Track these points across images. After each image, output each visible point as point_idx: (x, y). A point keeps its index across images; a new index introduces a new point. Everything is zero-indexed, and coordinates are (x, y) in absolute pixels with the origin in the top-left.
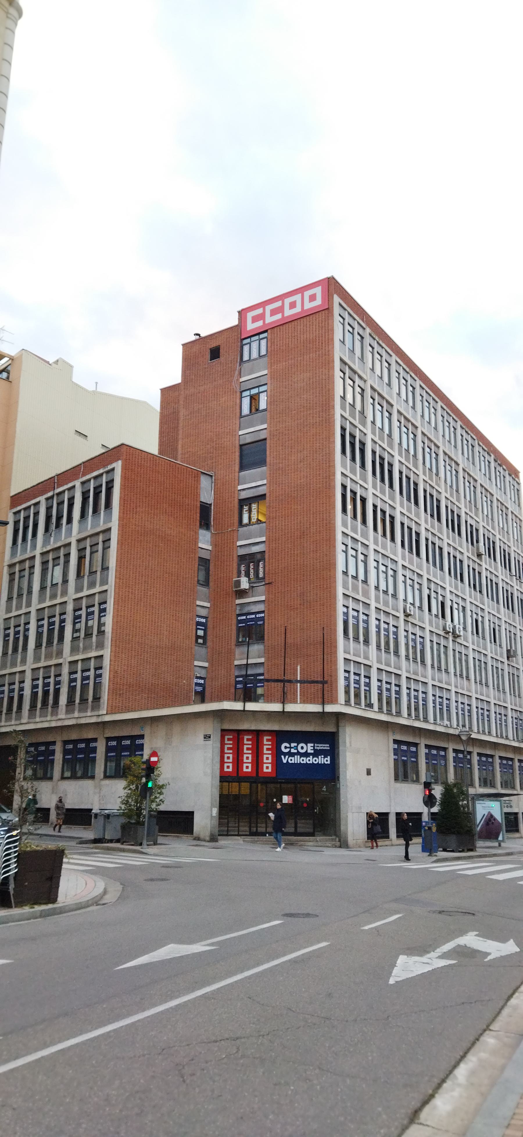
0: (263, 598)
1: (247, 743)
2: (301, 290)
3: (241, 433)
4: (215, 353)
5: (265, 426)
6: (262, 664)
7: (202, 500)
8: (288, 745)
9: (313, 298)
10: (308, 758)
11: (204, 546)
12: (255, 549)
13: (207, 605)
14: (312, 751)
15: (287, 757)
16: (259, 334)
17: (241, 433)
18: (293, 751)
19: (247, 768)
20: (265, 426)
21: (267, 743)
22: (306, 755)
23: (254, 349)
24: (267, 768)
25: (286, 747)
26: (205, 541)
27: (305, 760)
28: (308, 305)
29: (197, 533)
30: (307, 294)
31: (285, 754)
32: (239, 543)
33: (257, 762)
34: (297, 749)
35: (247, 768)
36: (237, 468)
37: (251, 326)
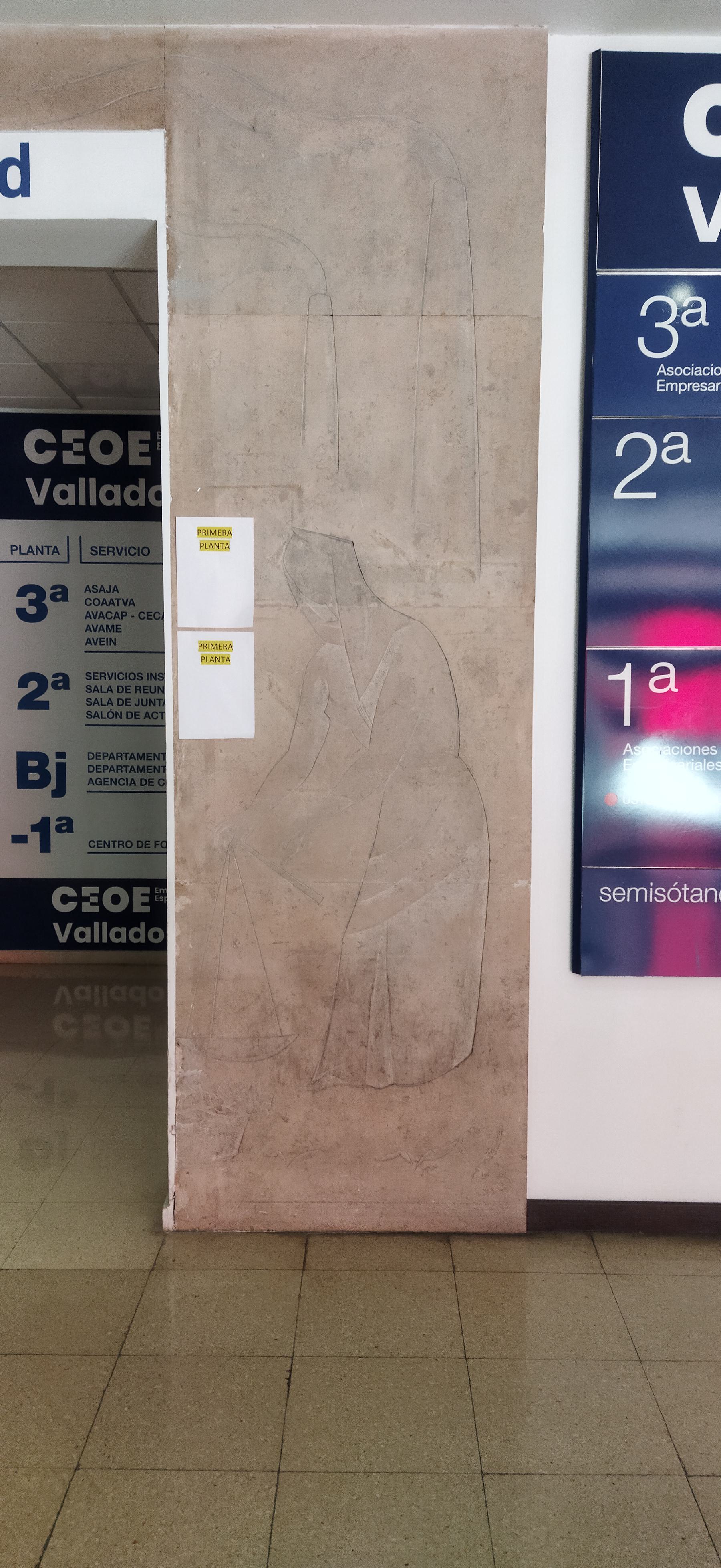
8: (48, 437)
10: (130, 489)
14: (147, 909)
15: (47, 482)
25: (41, 446)
34: (86, 452)
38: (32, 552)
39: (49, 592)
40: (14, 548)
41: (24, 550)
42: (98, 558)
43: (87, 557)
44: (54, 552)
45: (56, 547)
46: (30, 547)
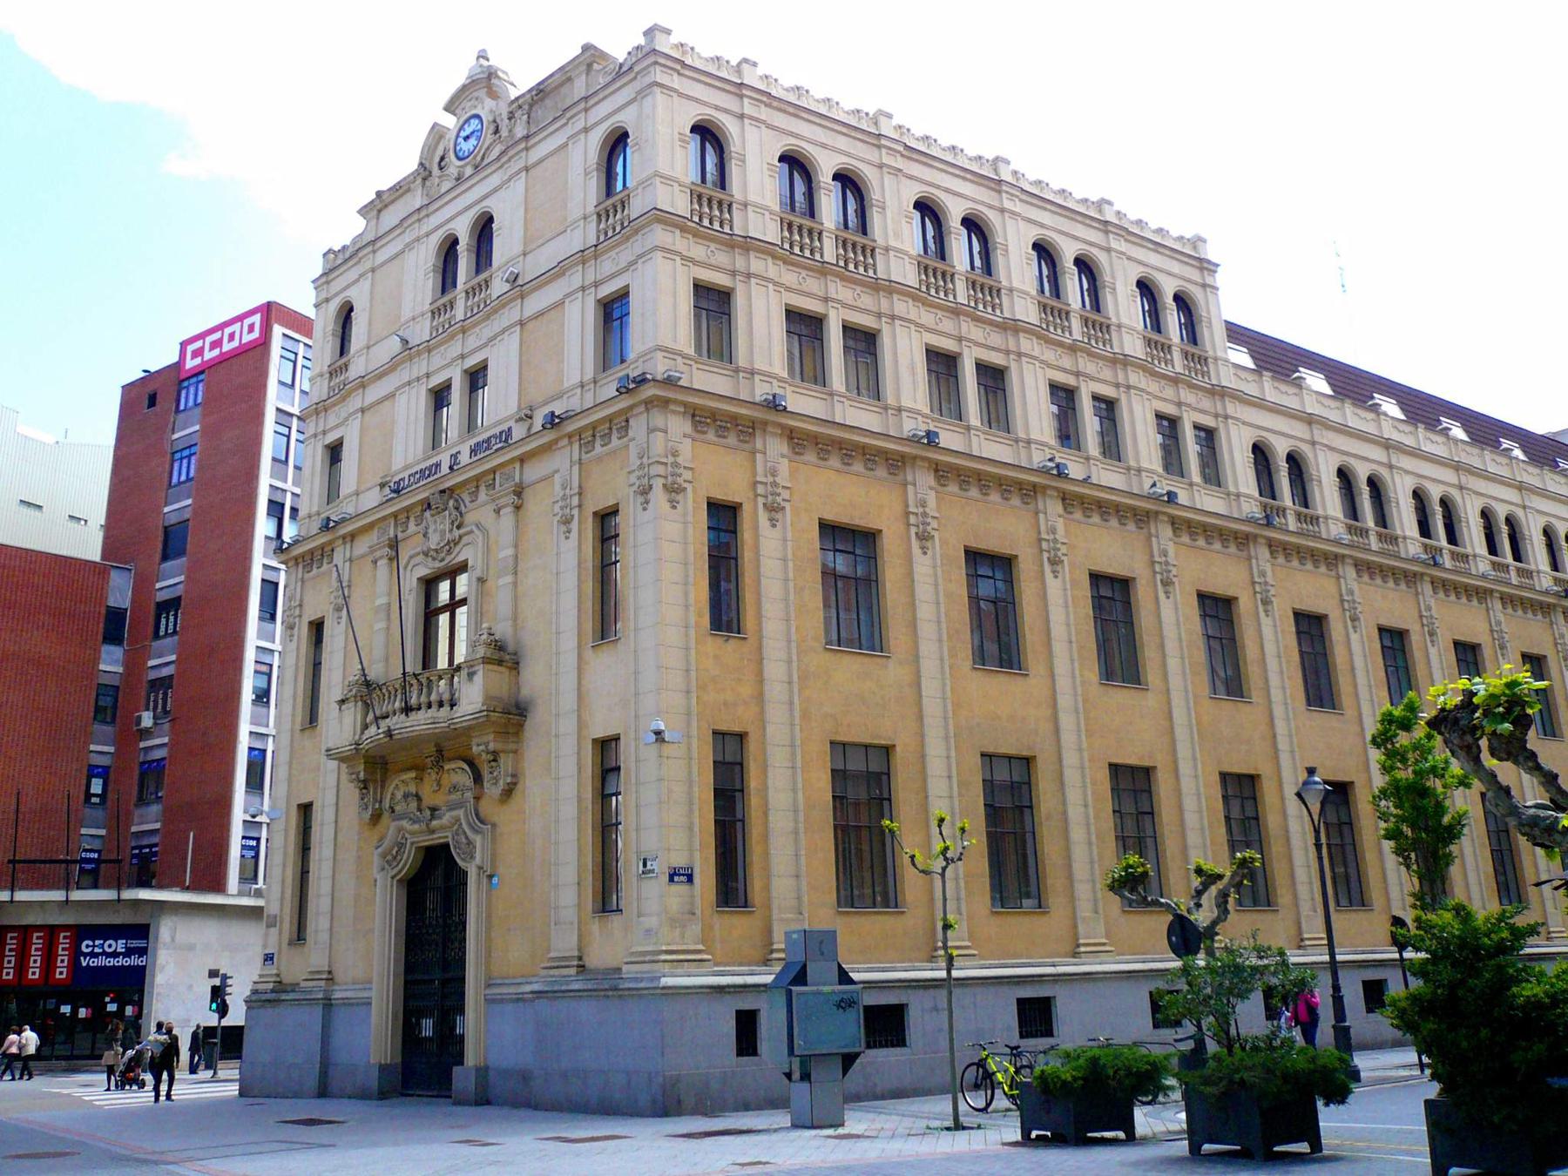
0: (166, 740)
1: (37, 941)
2: (240, 319)
3: (166, 510)
4: (152, 400)
5: (189, 501)
6: (157, 831)
7: (111, 603)
9: (251, 328)
11: (108, 668)
12: (165, 672)
13: (112, 749)
16: (196, 375)
17: (166, 510)
18: (97, 950)
19: (34, 973)
20: (189, 501)
21: (63, 942)
22: (115, 955)
23: (193, 395)
24: (61, 973)
26: (111, 662)
27: (111, 962)
28: (247, 338)
29: (97, 651)
30: (247, 322)
31: (85, 955)
32: (151, 663)
33: (22, 967)
35: (34, 973)
36: (158, 556)
37: (191, 363)
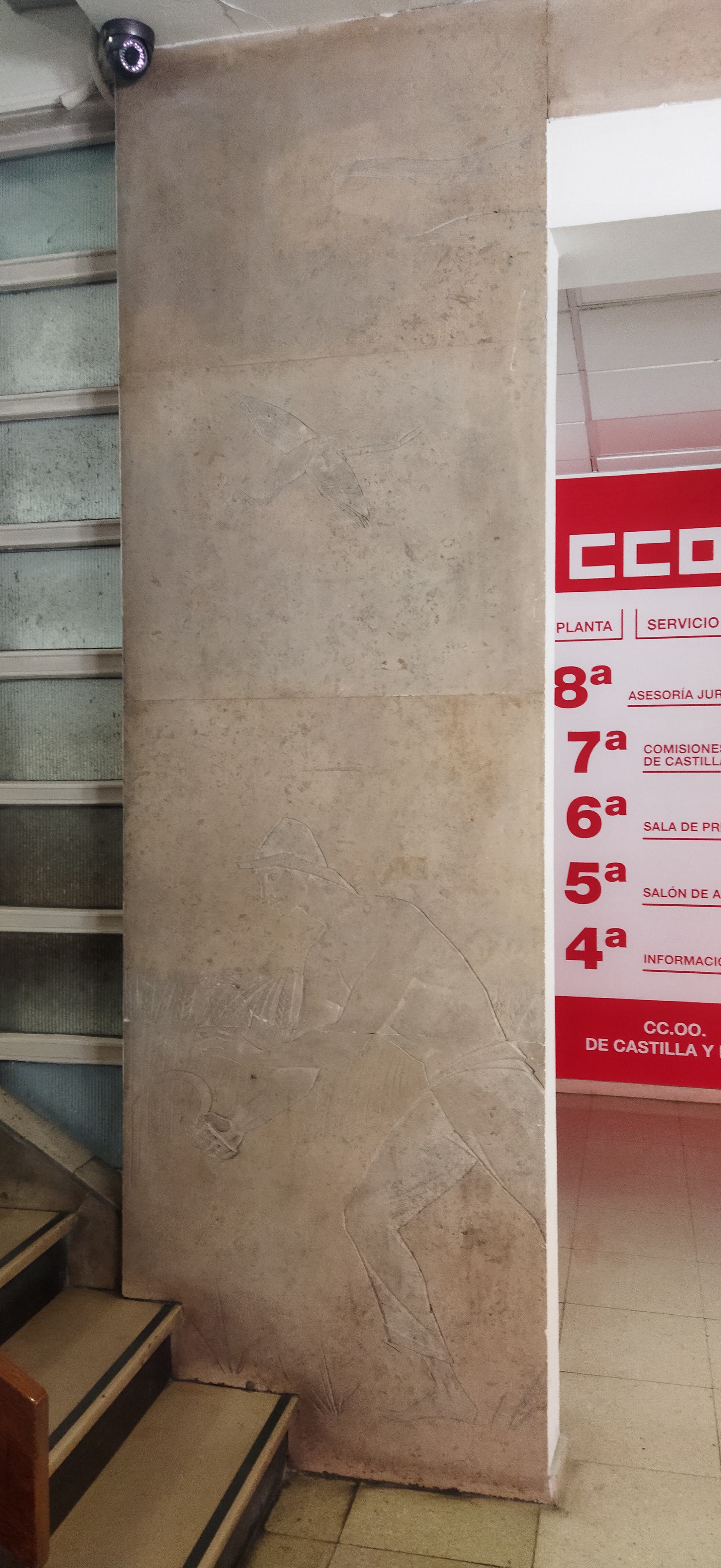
38: (581, 629)
39: (589, 674)
40: (561, 626)
41: (572, 627)
42: (657, 633)
43: (643, 631)
44: (605, 628)
45: (608, 622)
46: (579, 623)
